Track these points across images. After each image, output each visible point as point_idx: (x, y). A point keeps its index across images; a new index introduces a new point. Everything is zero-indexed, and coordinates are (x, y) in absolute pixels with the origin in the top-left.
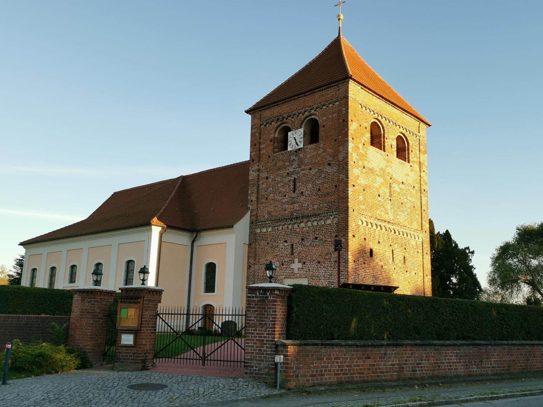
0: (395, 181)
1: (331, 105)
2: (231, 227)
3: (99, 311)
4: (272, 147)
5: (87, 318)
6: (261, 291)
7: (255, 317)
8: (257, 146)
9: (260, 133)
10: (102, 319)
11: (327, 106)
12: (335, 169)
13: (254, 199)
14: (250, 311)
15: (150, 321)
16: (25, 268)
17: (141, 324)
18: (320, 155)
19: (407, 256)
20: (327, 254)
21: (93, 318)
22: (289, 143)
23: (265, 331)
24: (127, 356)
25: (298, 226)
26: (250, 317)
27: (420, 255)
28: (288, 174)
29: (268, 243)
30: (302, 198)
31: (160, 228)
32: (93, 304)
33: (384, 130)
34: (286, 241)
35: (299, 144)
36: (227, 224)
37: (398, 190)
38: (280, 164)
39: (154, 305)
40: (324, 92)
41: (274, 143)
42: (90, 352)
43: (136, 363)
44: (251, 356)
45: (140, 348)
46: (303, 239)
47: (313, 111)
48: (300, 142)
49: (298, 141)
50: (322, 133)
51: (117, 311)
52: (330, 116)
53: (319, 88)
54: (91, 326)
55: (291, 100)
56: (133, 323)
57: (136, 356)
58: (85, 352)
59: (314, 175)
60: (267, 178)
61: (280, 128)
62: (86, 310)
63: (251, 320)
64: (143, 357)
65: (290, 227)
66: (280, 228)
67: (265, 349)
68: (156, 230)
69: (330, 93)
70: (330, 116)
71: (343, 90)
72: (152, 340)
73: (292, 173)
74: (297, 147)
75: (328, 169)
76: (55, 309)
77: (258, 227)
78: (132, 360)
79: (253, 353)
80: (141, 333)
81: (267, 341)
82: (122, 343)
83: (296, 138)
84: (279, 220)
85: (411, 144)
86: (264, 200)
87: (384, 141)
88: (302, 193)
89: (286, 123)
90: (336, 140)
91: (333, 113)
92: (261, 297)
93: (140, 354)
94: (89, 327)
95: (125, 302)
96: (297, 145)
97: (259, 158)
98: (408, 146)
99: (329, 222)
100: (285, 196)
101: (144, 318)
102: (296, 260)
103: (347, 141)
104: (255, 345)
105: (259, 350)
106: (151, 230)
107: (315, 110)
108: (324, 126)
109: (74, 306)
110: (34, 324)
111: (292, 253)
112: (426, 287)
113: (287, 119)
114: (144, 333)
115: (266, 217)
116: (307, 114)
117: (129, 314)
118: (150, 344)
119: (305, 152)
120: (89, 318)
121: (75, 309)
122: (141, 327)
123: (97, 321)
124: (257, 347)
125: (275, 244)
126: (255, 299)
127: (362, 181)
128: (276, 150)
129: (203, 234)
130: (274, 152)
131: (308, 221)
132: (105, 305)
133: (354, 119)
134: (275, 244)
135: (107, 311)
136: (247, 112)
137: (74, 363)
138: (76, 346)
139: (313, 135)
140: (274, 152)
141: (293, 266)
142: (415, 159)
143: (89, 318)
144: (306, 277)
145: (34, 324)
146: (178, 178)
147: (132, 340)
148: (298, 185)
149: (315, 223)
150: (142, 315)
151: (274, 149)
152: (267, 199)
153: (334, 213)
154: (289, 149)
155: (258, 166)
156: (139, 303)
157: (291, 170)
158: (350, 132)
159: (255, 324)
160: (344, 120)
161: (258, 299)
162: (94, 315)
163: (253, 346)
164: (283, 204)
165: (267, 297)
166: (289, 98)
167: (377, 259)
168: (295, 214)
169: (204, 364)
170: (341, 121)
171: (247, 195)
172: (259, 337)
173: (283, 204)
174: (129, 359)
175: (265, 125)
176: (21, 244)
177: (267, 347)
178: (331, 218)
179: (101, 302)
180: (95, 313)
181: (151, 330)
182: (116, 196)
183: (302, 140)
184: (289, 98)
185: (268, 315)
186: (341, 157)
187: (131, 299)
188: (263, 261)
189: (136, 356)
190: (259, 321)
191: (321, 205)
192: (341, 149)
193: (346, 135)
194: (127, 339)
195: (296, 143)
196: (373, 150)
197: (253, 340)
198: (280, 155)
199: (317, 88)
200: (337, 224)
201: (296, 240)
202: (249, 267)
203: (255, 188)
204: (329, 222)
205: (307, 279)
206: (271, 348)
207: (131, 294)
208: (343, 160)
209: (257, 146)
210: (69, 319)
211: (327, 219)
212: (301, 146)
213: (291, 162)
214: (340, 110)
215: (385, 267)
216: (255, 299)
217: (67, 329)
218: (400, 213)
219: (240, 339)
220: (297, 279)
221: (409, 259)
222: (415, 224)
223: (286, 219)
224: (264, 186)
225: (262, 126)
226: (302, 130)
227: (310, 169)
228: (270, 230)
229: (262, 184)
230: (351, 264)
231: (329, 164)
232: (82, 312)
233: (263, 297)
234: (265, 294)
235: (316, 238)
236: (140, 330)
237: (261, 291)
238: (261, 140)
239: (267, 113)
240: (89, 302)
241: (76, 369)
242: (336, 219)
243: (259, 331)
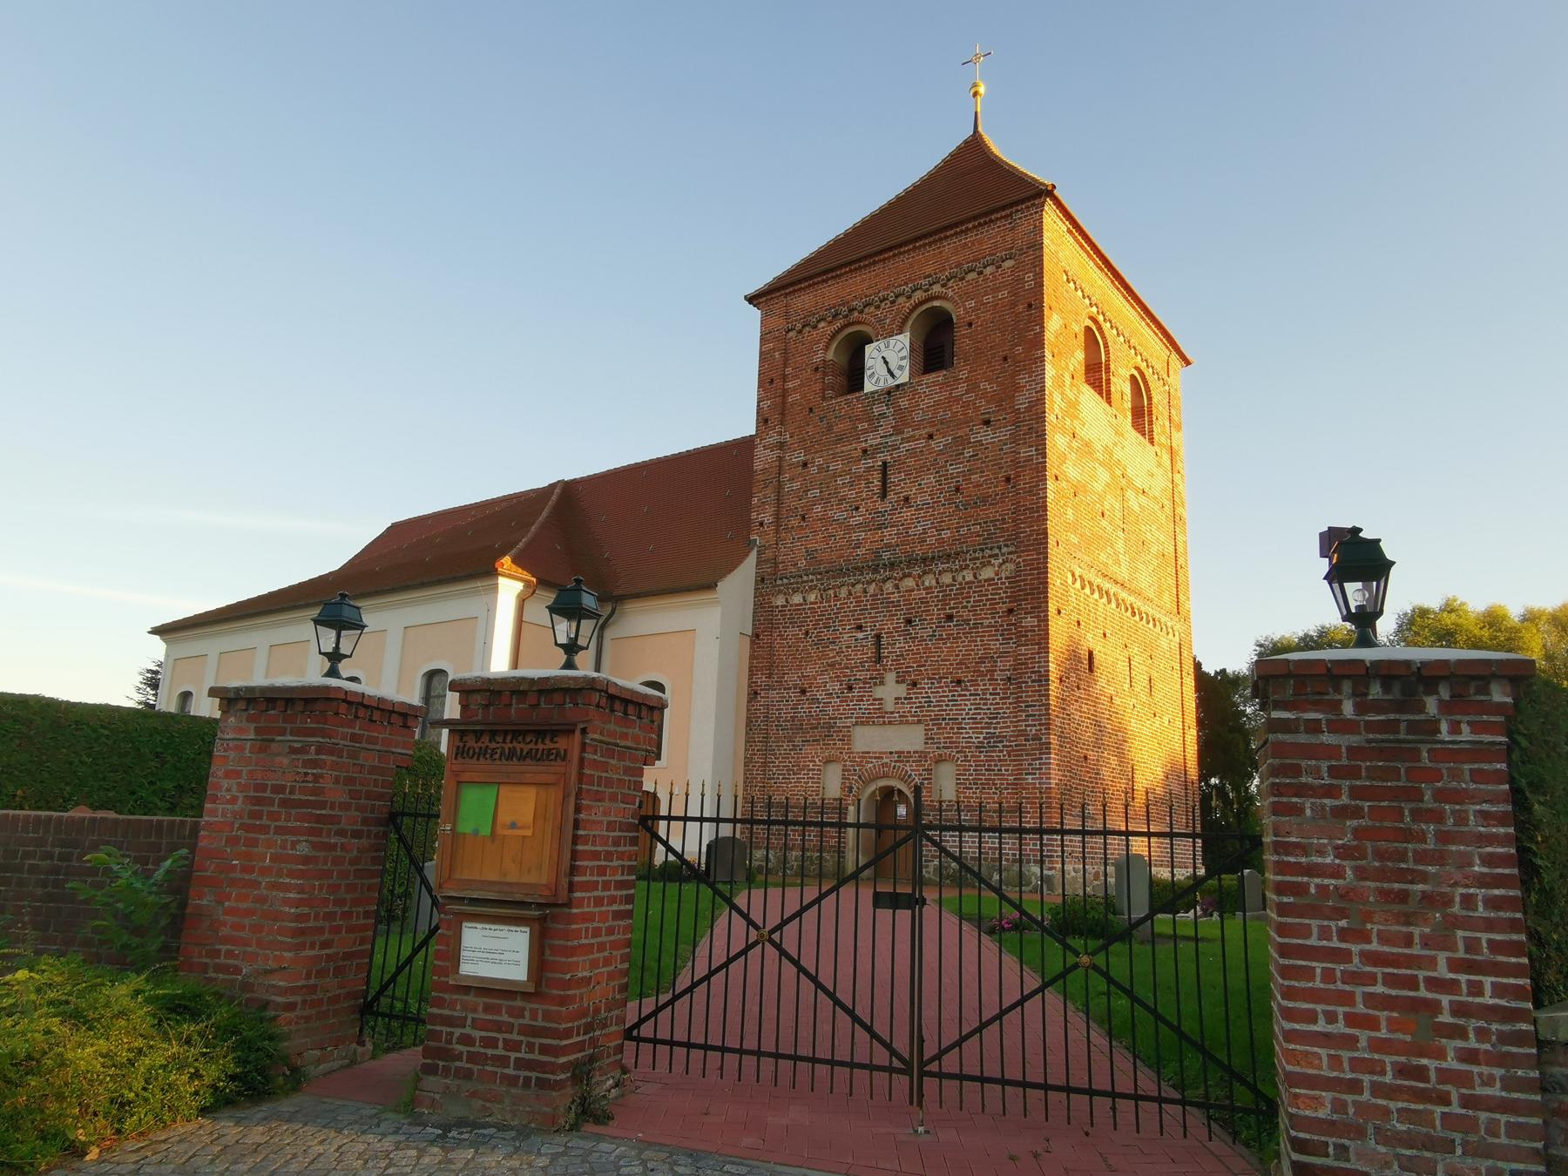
0: (1130, 483)
1: (989, 270)
2: (711, 586)
3: (345, 798)
4: (818, 387)
5: (280, 831)
6: (1375, 691)
7: (1343, 852)
8: (778, 383)
9: (785, 352)
10: (357, 834)
11: (980, 273)
12: (1004, 434)
13: (767, 518)
14: (1297, 811)
15: (609, 856)
16: (162, 690)
17: (573, 870)
18: (957, 399)
19: (1155, 675)
20: (982, 660)
21: (311, 832)
22: (868, 373)
23: (1447, 944)
24: (490, 1043)
25: (897, 587)
26: (1304, 849)
27: (1177, 675)
28: (865, 451)
29: (807, 633)
30: (907, 514)
31: (519, 586)
32: (314, 763)
33: (1107, 353)
34: (860, 628)
35: (897, 373)
36: (698, 581)
37: (1136, 508)
38: (840, 427)
39: (627, 770)
40: (971, 237)
41: (825, 374)
42: (290, 1007)
43: (542, 1084)
44: (1339, 1106)
45: (563, 1001)
46: (909, 622)
47: (937, 288)
48: (901, 368)
49: (893, 367)
50: (963, 340)
51: (433, 801)
52: (988, 298)
53: (956, 225)
54: (301, 875)
55: (875, 263)
56: (533, 872)
57: (544, 1050)
58: (265, 1005)
59: (941, 453)
60: (805, 465)
61: (840, 336)
62: (278, 789)
63: (1311, 871)
64: (580, 1047)
65: (872, 588)
66: (843, 592)
67: (1451, 1063)
68: (509, 589)
69: (989, 237)
70: (988, 298)
71: (1025, 226)
72: (617, 953)
73: (877, 449)
74: (891, 382)
75: (985, 436)
76: (179, 787)
77: (780, 592)
78: (520, 1064)
79: (1355, 1087)
80: (571, 919)
81: (1459, 1010)
82: (466, 969)
83: (889, 359)
84: (841, 573)
85: (1155, 400)
86: (794, 522)
87: (1108, 381)
88: (907, 499)
89: (859, 323)
90: (1005, 359)
91: (996, 290)
92: (1370, 726)
93: (567, 1033)
94: (291, 874)
95: (482, 753)
96: (892, 375)
97: (783, 414)
98: (1150, 404)
99: (988, 573)
100: (857, 509)
101: (585, 840)
102: (890, 677)
103: (1042, 359)
104: (1364, 1036)
105: (1402, 1071)
106: (495, 588)
107: (944, 286)
108: (970, 325)
109: (218, 770)
110: (27, 855)
111: (879, 659)
112: (1189, 756)
113: (861, 312)
114: (588, 918)
115: (802, 564)
116: (919, 295)
117: (505, 818)
118: (611, 976)
119: (915, 392)
120: (292, 831)
121: (225, 783)
122: (571, 887)
123: (333, 847)
124: (1378, 1045)
125: (826, 634)
126: (1327, 738)
127: (1071, 471)
128: (829, 393)
129: (631, 607)
130: (824, 399)
131: (925, 573)
132: (373, 770)
133: (1054, 304)
134: (826, 634)
135: (380, 797)
136: (752, 299)
137: (196, 1075)
138: (220, 968)
139: (935, 349)
140: (824, 399)
141: (879, 692)
142: (1163, 440)
143: (292, 831)
144: (919, 722)
145: (27, 855)
146: (553, 486)
147: (523, 956)
148: (893, 479)
149: (947, 579)
150: (577, 824)
151: (823, 390)
152: (803, 518)
153: (1004, 550)
154: (869, 387)
155: (780, 433)
156: (563, 757)
157: (873, 440)
158: (1049, 336)
159: (1344, 895)
160: (1030, 306)
161: (1354, 740)
162: (319, 819)
163: (1350, 1042)
164: (850, 529)
165: (1432, 727)
166: (871, 256)
167: (1102, 681)
168: (886, 556)
169: (917, 1097)
170: (1021, 308)
171: (748, 508)
172: (1390, 980)
173: (850, 529)
174: (503, 1061)
175: (800, 332)
176: (156, 631)
177: (1470, 1056)
178: (996, 563)
179: (353, 755)
180: (322, 805)
181: (612, 900)
182: (396, 530)
183: (906, 363)
184: (871, 256)
185: (1444, 838)
186: (1022, 402)
187: (517, 734)
188: (792, 678)
189: (544, 1050)
190: (1381, 875)
191: (964, 531)
192: (1023, 379)
193: (1038, 342)
194: (496, 953)
195: (889, 371)
196: (1088, 395)
197: (1348, 999)
198: (841, 403)
199: (950, 227)
200: (1013, 580)
201: (889, 624)
202: (753, 695)
203: (768, 491)
204: (988, 573)
205: (922, 727)
206: (1501, 1060)
207: (516, 709)
208: (1028, 409)
209: (778, 383)
210: (195, 828)
211: (984, 565)
212: (903, 377)
213: (873, 422)
214: (1021, 280)
215: (1117, 701)
216: (1327, 738)
217: (180, 885)
218: (1140, 566)
219: (758, 894)
220: (890, 731)
221: (1158, 685)
222: (1166, 597)
223: (860, 570)
224: (797, 485)
225: (791, 334)
226: (904, 339)
227: (931, 437)
228: (812, 597)
229: (792, 480)
230: (1054, 687)
231: (987, 423)
232: (258, 801)
233: (1391, 726)
234: (1410, 703)
235: (950, 618)
236: (569, 904)
237: (1375, 691)
238: (789, 370)
239: (804, 301)
240: (293, 751)
241: (203, 1111)
242: (1011, 567)
243: (1384, 938)
